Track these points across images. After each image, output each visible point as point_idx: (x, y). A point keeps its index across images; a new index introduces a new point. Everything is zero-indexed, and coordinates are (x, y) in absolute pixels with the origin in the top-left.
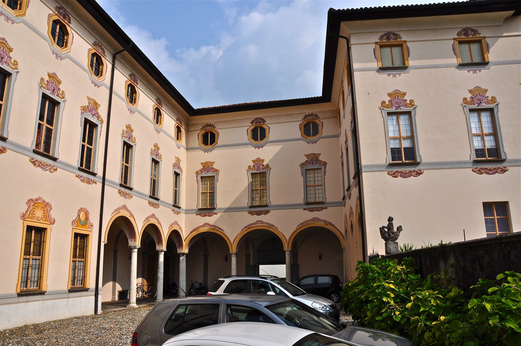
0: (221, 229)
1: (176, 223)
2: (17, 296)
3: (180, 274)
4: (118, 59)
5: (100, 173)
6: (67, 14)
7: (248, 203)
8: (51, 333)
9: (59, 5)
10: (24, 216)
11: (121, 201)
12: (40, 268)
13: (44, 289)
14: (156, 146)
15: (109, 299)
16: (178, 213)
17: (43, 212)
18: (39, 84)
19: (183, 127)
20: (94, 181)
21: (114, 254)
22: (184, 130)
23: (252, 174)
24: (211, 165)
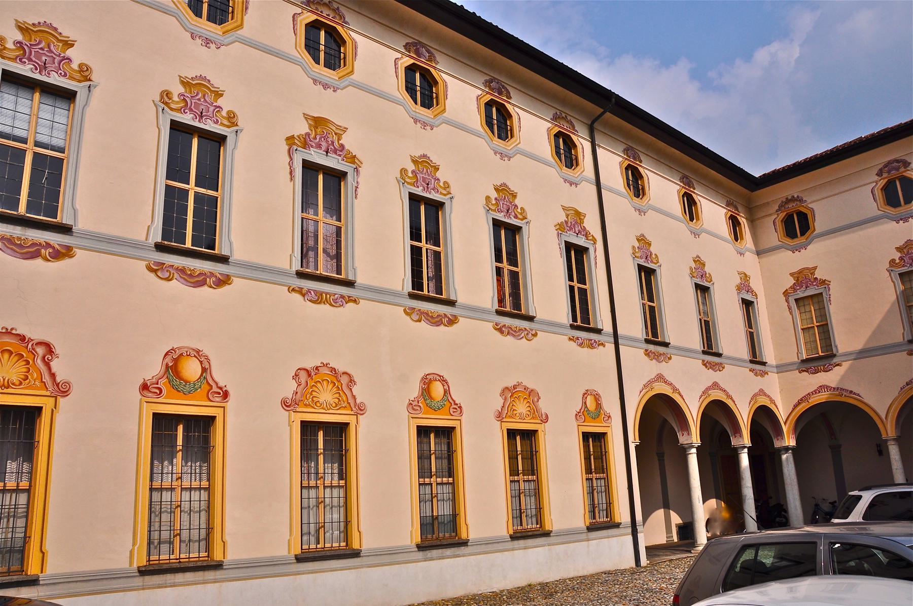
0: (855, 394)
1: (762, 392)
2: (510, 539)
3: (786, 486)
4: (599, 130)
5: (608, 327)
6: (503, 87)
7: (903, 334)
8: (566, 596)
9: (487, 78)
10: (500, 416)
11: (652, 368)
12: (537, 494)
13: (548, 527)
14: (698, 261)
15: (662, 539)
16: (763, 374)
17: (528, 405)
18: (484, 208)
19: (741, 214)
20: (600, 342)
21: (659, 460)
22: (744, 220)
23: (901, 275)
24: (811, 274)
